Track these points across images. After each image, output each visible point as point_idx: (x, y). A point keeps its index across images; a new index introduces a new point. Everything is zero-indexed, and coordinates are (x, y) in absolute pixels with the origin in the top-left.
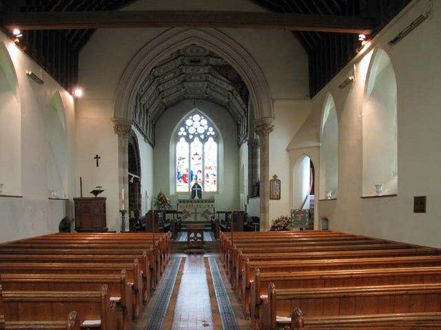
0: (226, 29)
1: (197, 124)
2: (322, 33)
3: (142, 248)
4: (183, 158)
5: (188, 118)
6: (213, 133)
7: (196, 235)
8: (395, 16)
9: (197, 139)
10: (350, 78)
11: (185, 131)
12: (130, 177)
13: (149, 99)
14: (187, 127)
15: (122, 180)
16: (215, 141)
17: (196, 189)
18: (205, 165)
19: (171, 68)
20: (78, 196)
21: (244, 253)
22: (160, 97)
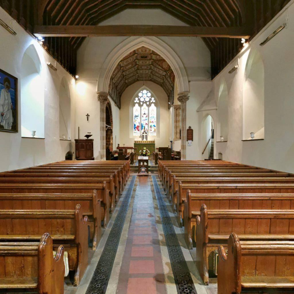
0: (162, 37)
1: (145, 95)
2: (219, 38)
3: (114, 169)
4: (137, 116)
5: (140, 92)
6: (154, 101)
7: (143, 163)
8: (264, 27)
9: (145, 105)
10: (236, 67)
11: (138, 100)
12: (106, 127)
13: (118, 79)
14: (139, 98)
15: (102, 128)
16: (155, 106)
17: (145, 135)
18: (150, 120)
19: (130, 62)
20: (77, 138)
21: (172, 172)
22: (124, 79)
